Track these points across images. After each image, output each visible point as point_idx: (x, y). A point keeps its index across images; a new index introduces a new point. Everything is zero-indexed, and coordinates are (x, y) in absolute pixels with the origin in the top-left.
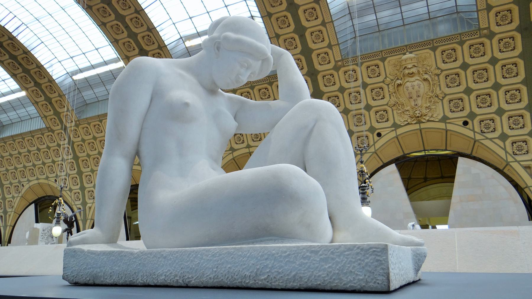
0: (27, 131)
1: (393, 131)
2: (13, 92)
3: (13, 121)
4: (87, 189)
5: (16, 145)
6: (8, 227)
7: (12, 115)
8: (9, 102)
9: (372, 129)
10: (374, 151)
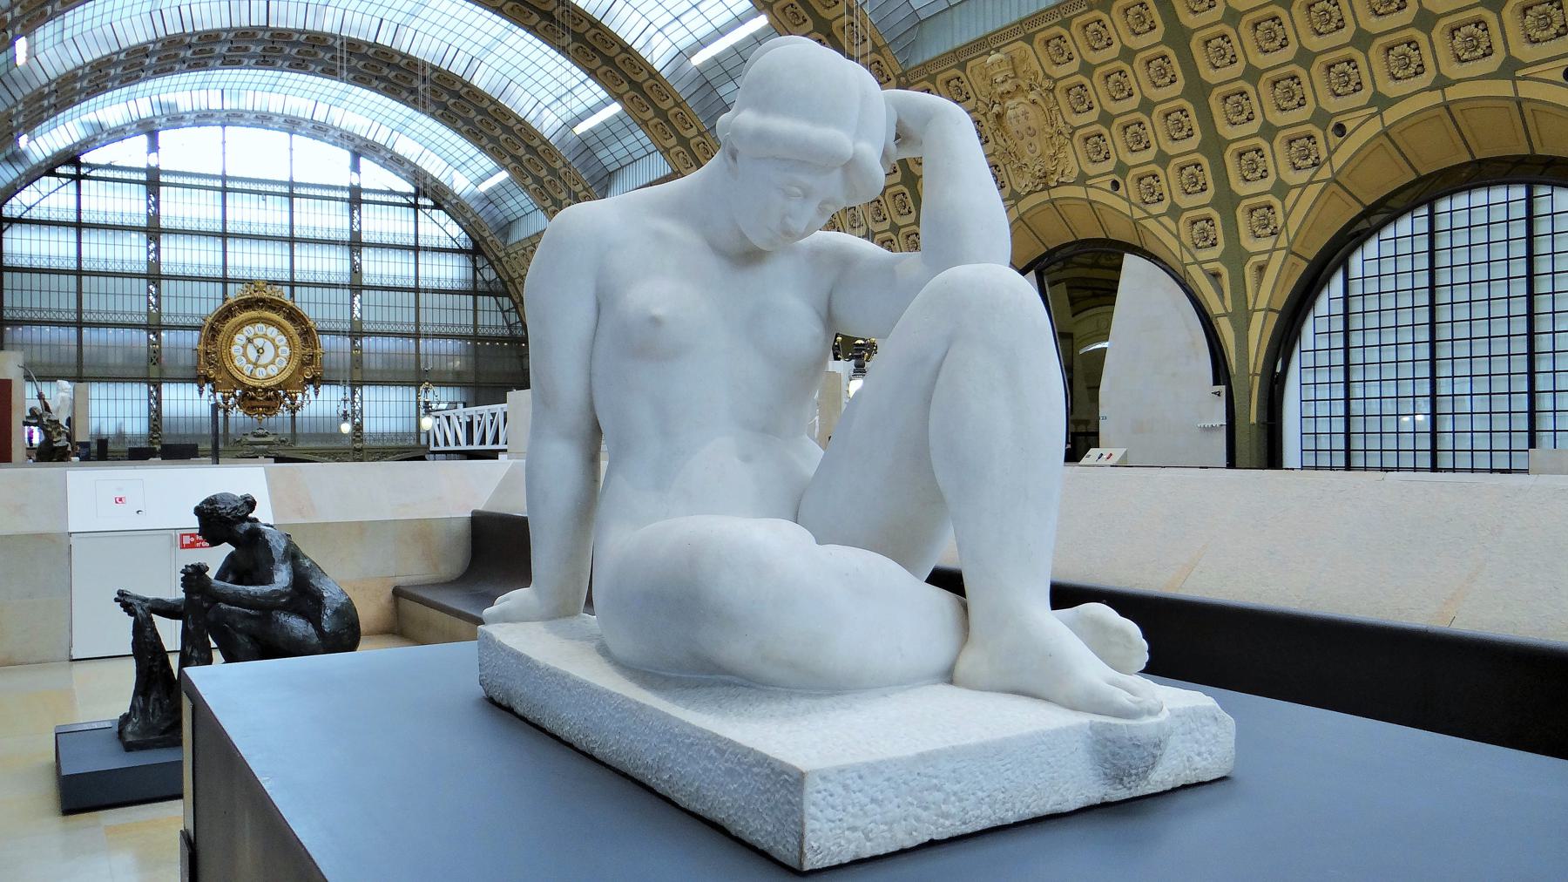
1: (1373, 116)
6: (1257, 319)
9: (1320, 117)
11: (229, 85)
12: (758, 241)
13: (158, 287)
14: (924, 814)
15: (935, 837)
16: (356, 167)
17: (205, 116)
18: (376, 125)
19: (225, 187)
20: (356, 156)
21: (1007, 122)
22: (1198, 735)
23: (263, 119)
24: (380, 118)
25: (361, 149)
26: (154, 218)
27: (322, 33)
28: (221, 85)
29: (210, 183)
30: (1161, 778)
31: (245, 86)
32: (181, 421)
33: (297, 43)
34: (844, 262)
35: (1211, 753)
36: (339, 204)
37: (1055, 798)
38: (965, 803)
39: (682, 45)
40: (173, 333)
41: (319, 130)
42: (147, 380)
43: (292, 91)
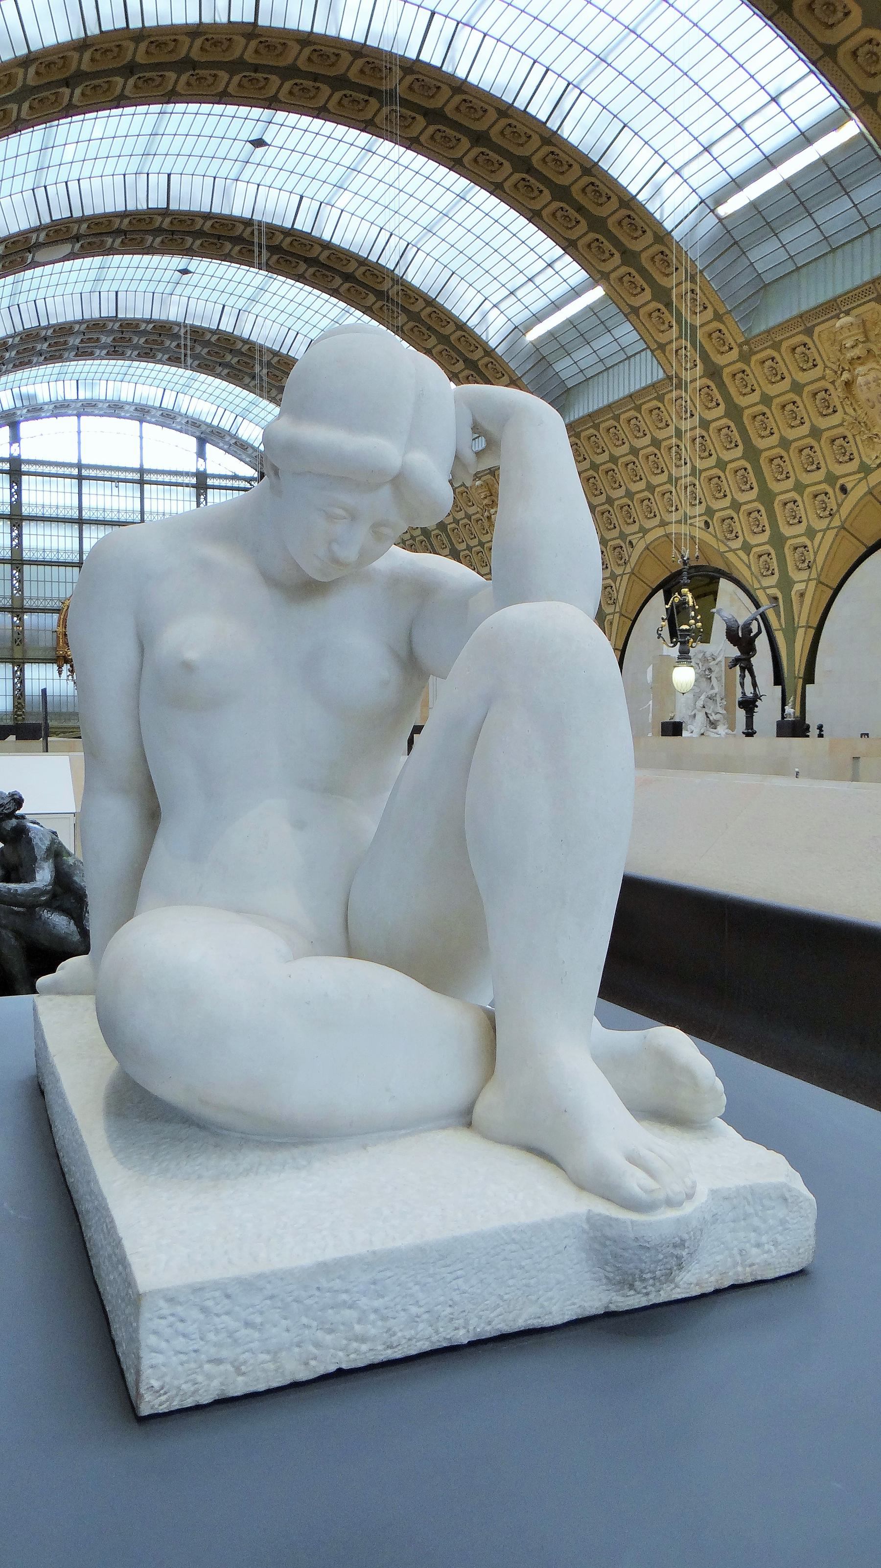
0: (621, 395)
2: (576, 293)
3: (589, 373)
4: (790, 542)
5: (604, 439)
6: (801, 632)
7: (584, 356)
8: (571, 322)
10: (839, 524)
11: (83, 376)
12: (313, 569)
13: (21, 571)
14: (329, 1338)
15: (344, 1366)
16: (201, 453)
17: (62, 406)
18: (221, 411)
19: (81, 474)
20: (202, 442)
21: (856, 390)
22: (756, 1221)
23: (115, 409)
24: (225, 404)
25: (206, 435)
26: (17, 505)
27: (167, 322)
28: (76, 376)
29: (67, 471)
30: (691, 1281)
31: (98, 376)
32: (64, 699)
33: (144, 333)
34: (423, 590)
35: (776, 1244)
36: (187, 489)
37: (533, 1310)
38: (390, 1323)
39: (517, 321)
40: (34, 616)
41: (167, 418)
42: (12, 661)
43: (142, 379)
